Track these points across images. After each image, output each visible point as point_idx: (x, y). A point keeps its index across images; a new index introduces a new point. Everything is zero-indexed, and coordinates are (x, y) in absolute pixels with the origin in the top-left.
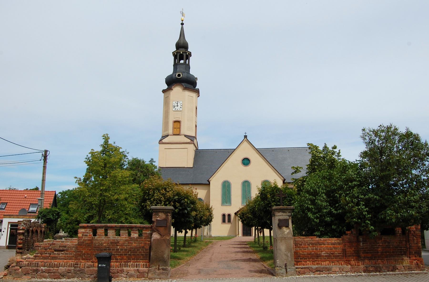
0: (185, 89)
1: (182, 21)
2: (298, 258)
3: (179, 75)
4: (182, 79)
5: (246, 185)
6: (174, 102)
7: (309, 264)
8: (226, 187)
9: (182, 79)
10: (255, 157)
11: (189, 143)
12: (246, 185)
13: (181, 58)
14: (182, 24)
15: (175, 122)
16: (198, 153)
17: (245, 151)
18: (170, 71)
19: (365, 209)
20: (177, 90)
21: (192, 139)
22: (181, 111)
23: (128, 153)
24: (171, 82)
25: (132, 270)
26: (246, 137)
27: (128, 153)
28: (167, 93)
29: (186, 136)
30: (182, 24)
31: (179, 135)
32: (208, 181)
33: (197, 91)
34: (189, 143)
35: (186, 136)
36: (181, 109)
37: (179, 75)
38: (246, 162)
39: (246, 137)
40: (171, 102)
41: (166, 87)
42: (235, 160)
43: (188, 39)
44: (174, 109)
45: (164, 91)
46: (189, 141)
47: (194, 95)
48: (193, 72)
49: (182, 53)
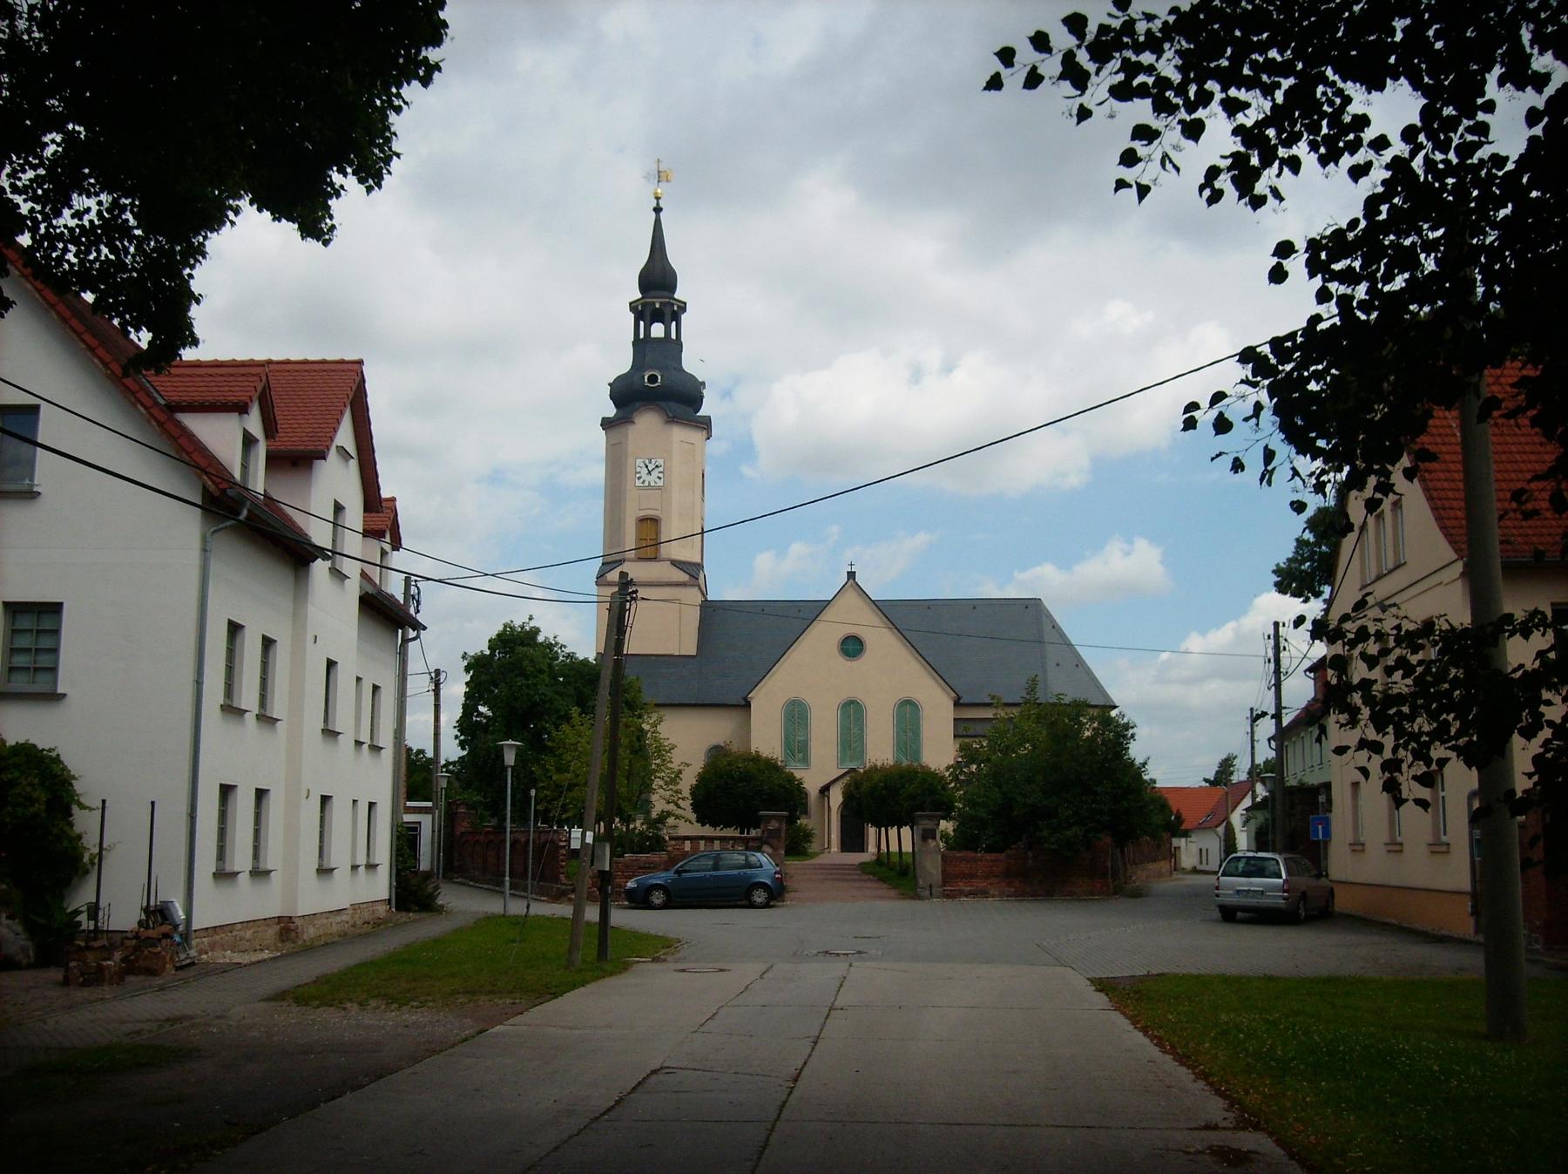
0: (673, 419)
1: (658, 198)
2: (947, 878)
3: (653, 379)
4: (657, 390)
5: (852, 712)
6: (639, 462)
7: (962, 886)
8: (796, 715)
9: (657, 390)
10: (881, 640)
11: (684, 584)
12: (852, 712)
13: (657, 316)
14: (658, 210)
15: (643, 520)
16: (712, 612)
17: (852, 618)
18: (623, 362)
19: (17, 774)
20: (647, 422)
21: (693, 570)
22: (659, 488)
23: (531, 618)
24: (630, 397)
25: (255, 1033)
26: (851, 575)
27: (531, 618)
28: (617, 433)
29: (674, 563)
30: (658, 210)
31: (654, 559)
32: (745, 699)
33: (705, 425)
34: (684, 584)
35: (674, 563)
36: (660, 483)
37: (653, 379)
38: (852, 647)
39: (851, 575)
40: (630, 460)
41: (611, 411)
42: (821, 639)
43: (674, 257)
44: (638, 483)
45: (607, 424)
46: (684, 577)
47: (696, 436)
48: (691, 362)
49: (657, 293)
